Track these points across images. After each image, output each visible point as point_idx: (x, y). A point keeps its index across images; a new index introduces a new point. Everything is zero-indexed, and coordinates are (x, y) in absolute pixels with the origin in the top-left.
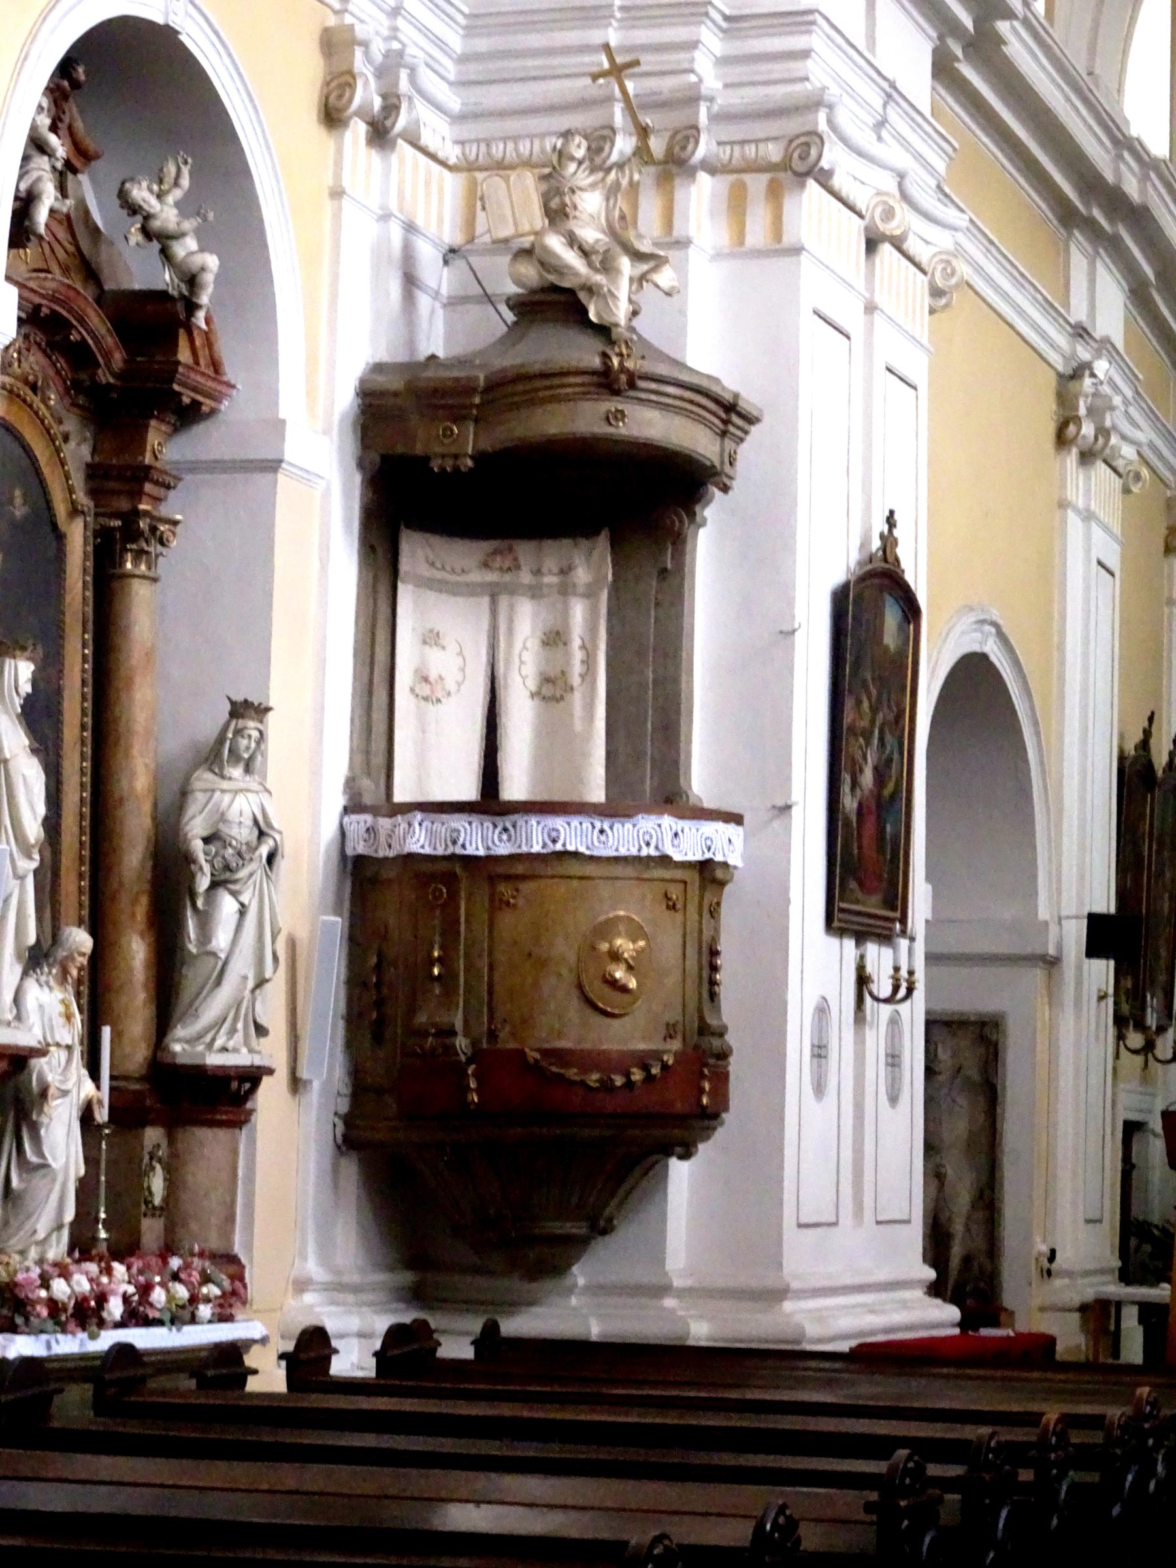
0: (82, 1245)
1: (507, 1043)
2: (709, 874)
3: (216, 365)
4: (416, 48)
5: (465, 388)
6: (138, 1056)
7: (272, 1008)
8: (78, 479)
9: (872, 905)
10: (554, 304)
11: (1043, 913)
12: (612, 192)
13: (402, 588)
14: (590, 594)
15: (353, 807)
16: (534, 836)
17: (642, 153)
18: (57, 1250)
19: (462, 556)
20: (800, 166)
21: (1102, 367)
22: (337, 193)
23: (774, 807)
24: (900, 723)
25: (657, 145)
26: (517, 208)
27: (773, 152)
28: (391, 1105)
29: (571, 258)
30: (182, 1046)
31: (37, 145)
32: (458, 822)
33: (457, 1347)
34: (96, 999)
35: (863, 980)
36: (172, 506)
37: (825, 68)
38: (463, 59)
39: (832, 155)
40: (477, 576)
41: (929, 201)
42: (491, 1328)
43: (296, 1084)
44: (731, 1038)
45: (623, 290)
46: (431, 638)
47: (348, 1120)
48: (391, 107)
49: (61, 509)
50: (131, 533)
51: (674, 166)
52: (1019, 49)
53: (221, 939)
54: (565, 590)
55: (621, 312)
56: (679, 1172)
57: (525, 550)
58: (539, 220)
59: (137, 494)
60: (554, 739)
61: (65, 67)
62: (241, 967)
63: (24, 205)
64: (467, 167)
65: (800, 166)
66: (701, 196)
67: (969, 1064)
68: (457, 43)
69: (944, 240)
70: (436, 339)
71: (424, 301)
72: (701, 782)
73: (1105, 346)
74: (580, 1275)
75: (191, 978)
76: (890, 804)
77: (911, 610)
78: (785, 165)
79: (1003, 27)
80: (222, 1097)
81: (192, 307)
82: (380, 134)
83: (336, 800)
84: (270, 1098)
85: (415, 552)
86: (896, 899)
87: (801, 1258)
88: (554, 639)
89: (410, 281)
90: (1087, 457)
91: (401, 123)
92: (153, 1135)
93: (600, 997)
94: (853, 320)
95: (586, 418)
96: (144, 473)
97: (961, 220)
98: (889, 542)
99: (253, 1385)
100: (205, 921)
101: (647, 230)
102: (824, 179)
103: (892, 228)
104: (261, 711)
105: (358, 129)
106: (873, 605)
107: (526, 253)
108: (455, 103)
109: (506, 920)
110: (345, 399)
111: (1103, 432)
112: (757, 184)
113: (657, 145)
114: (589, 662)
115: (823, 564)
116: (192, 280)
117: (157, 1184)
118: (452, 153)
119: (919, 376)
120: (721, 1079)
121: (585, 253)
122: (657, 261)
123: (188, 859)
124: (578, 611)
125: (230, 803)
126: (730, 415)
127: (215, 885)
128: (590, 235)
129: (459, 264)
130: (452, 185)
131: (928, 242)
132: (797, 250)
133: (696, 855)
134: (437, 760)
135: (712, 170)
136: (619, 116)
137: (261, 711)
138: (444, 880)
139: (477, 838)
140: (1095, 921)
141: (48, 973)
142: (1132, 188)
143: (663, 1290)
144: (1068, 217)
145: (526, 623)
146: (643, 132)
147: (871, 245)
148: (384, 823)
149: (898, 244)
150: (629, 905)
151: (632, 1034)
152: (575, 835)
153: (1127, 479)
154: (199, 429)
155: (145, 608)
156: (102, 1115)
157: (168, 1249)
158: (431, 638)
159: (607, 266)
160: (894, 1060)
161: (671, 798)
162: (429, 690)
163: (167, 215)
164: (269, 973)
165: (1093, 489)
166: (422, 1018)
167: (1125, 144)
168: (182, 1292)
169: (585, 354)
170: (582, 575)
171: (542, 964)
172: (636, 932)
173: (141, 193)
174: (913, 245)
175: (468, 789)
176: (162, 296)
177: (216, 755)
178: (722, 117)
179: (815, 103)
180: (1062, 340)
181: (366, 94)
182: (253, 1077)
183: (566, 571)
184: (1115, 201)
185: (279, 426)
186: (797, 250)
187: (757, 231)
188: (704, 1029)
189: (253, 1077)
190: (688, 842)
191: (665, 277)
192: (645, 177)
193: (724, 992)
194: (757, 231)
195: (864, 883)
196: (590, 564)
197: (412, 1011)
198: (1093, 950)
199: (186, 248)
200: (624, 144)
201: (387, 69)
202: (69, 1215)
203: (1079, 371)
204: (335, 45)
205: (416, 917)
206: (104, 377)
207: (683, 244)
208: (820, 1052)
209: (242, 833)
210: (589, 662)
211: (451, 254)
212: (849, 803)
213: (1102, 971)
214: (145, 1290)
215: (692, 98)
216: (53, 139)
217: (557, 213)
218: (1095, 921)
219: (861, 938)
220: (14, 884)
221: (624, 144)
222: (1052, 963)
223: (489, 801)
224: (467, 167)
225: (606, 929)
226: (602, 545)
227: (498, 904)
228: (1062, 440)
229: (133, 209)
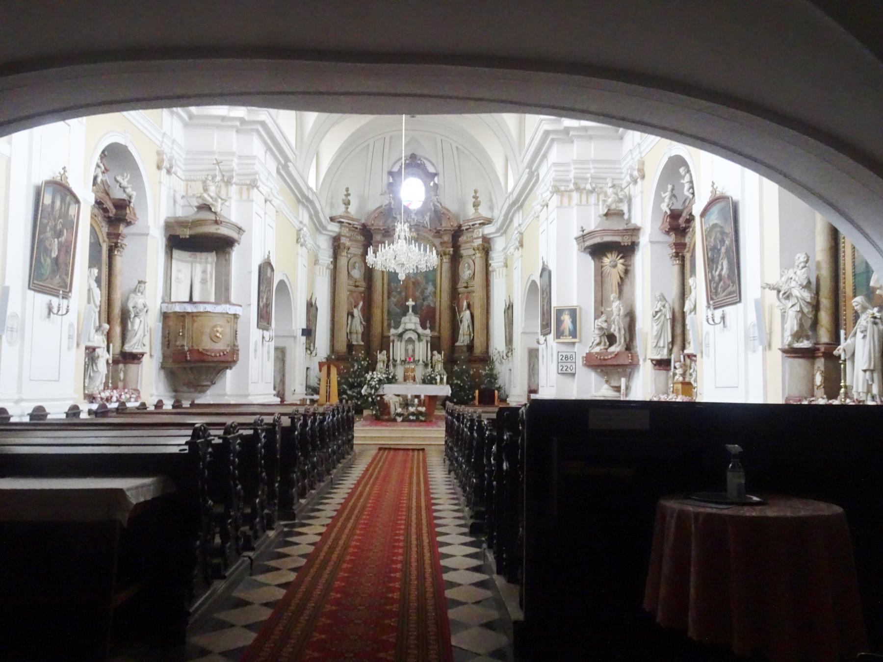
0: (106, 386)
1: (195, 348)
2: (236, 316)
3: (135, 214)
4: (176, 156)
5: (188, 222)
6: (118, 350)
7: (146, 341)
8: (105, 235)
9: (265, 324)
10: (205, 207)
11: (294, 328)
12: (217, 187)
13: (174, 261)
14: (211, 263)
15: (163, 302)
16: (201, 308)
17: (223, 180)
18: (102, 387)
19: (186, 255)
20: (253, 185)
21: (305, 229)
22: (160, 183)
23: (643, 163)
24: (270, 291)
25: (226, 179)
26: (198, 189)
27: (248, 182)
28: (171, 360)
29: (209, 198)
30: (128, 348)
31: (98, 166)
32: (186, 305)
33: (186, 404)
34: (109, 337)
35: (263, 337)
36: (125, 241)
37: (258, 167)
38: (186, 159)
39: (259, 184)
40: (189, 259)
41: (276, 194)
42: (193, 402)
43: (151, 356)
44: (240, 347)
45: (219, 205)
46: (179, 271)
47: (162, 364)
48: (171, 167)
49: (101, 241)
50: (116, 245)
51: (228, 183)
52: (292, 169)
53: (136, 327)
54: (206, 262)
55: (218, 210)
56: (228, 371)
57: (198, 254)
58: (202, 191)
59: (118, 239)
60: (204, 290)
61: (103, 152)
62: (140, 333)
63: (95, 178)
64: (187, 180)
65: (253, 185)
66: (233, 189)
67: (281, 354)
68: (184, 156)
69: (278, 201)
70: (180, 213)
71: (177, 205)
72: (233, 299)
73: (305, 225)
74: (208, 392)
75: (129, 335)
76: (268, 305)
77: (273, 270)
78: (250, 185)
79: (289, 164)
80: (134, 358)
81: (130, 202)
82: (169, 172)
83: (159, 301)
84: (145, 359)
85: (176, 253)
86: (269, 323)
87: (252, 389)
88: (204, 272)
89: (175, 202)
90: (302, 245)
91: (173, 170)
92: (121, 366)
93: (214, 339)
94: (263, 215)
95: (212, 229)
96: (119, 235)
97: (281, 198)
98: (269, 256)
99: (164, 407)
100: (132, 323)
101: (223, 194)
102: (258, 188)
103: (270, 199)
104: (145, 283)
105: (164, 171)
106: (266, 268)
107: (200, 197)
108: (183, 168)
109: (196, 324)
110: (162, 223)
111: (305, 241)
112: (245, 188)
113: (226, 179)
114: (211, 276)
115: (257, 260)
116: (130, 197)
117: (122, 376)
118: (183, 177)
119: (274, 226)
120: (238, 354)
121: (212, 198)
122: (226, 200)
123: (129, 311)
124: (209, 266)
125: (136, 301)
126: (240, 230)
127: (135, 316)
128: (213, 194)
129: (185, 199)
130: (183, 184)
131: (276, 202)
132: (252, 201)
133: (233, 312)
134: (180, 293)
135: (236, 184)
136: (217, 173)
137: (145, 283)
138: (182, 316)
139: (189, 308)
140: (303, 330)
141: (100, 333)
142: (310, 197)
143: (225, 395)
144: (299, 201)
145: (198, 268)
146: (223, 176)
147: (266, 201)
148: (170, 305)
149: (270, 201)
150: (220, 321)
151: (220, 346)
152: (209, 308)
153: (309, 250)
154: (131, 227)
155: (120, 261)
156: (110, 361)
157: (124, 388)
158: (179, 271)
159: (216, 201)
160: (268, 353)
161: (227, 301)
162: (178, 280)
163: (124, 183)
164: (146, 335)
165: (303, 251)
166: (178, 343)
167: (309, 188)
168: (128, 396)
169: (212, 217)
170: (210, 259)
171: (202, 333)
172: (221, 327)
173: (119, 178)
174: (273, 202)
175: (187, 299)
176: (124, 200)
177: (135, 291)
178: (238, 175)
179: (256, 173)
180: (298, 224)
181: (166, 164)
182: (143, 354)
183: (207, 259)
184: (307, 199)
185: (148, 227)
186: (252, 201)
187: (245, 196)
188: (234, 345)
189: (143, 354)
190: (232, 310)
191: (227, 204)
192: (223, 184)
193: (238, 338)
194: (245, 196)
195: (264, 318)
196: (211, 257)
197: (176, 341)
198: (303, 334)
199: (129, 190)
200: (218, 178)
201: (170, 160)
202: (104, 381)
203: (300, 230)
204: (159, 153)
205: (175, 323)
206: (111, 215)
207: (230, 198)
208: (256, 350)
209: (140, 306)
210: (211, 276)
211: (183, 197)
212: (261, 305)
213: (304, 338)
214: (121, 395)
215: (232, 171)
216: (101, 165)
217: (206, 190)
218: (303, 330)
219: (263, 329)
220: (93, 313)
221: (218, 178)
222: (295, 337)
223: (191, 301)
224: (187, 180)
225: (215, 326)
226: (214, 253)
227: (194, 321)
228: (297, 242)
229: (117, 182)
